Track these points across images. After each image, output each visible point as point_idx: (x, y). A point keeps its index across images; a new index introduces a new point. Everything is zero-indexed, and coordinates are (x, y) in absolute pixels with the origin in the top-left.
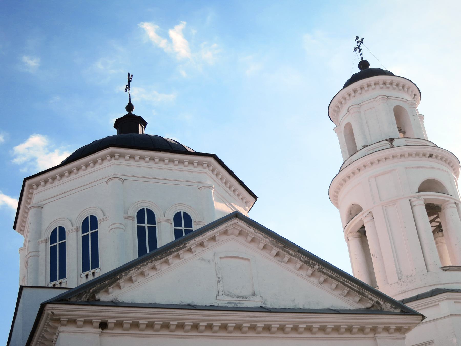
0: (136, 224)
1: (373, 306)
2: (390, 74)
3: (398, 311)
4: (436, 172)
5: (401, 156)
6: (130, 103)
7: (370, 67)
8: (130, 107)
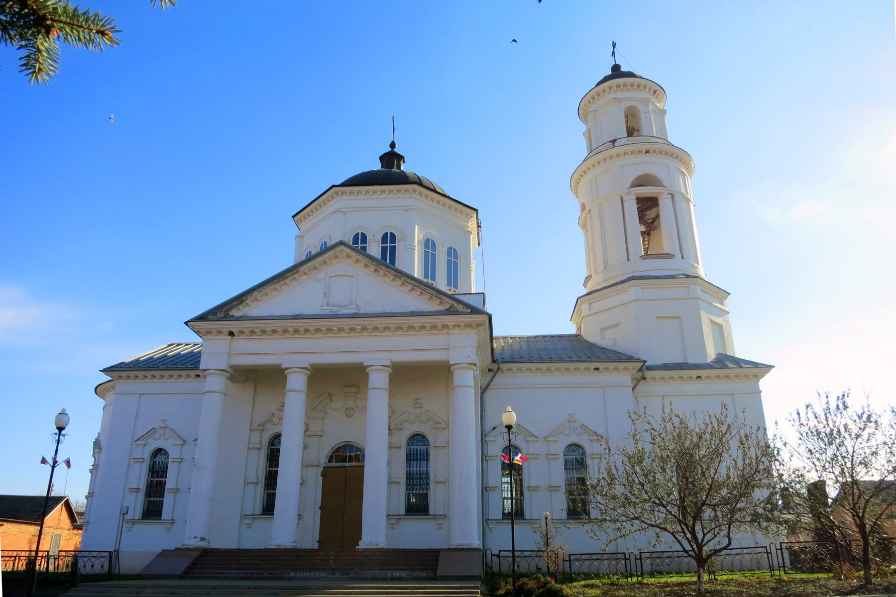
1: (451, 307)
3: (469, 311)
5: (632, 153)
8: (393, 145)
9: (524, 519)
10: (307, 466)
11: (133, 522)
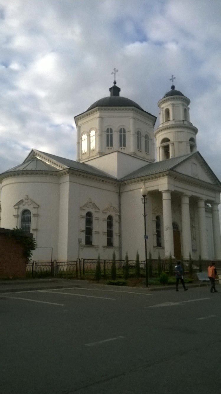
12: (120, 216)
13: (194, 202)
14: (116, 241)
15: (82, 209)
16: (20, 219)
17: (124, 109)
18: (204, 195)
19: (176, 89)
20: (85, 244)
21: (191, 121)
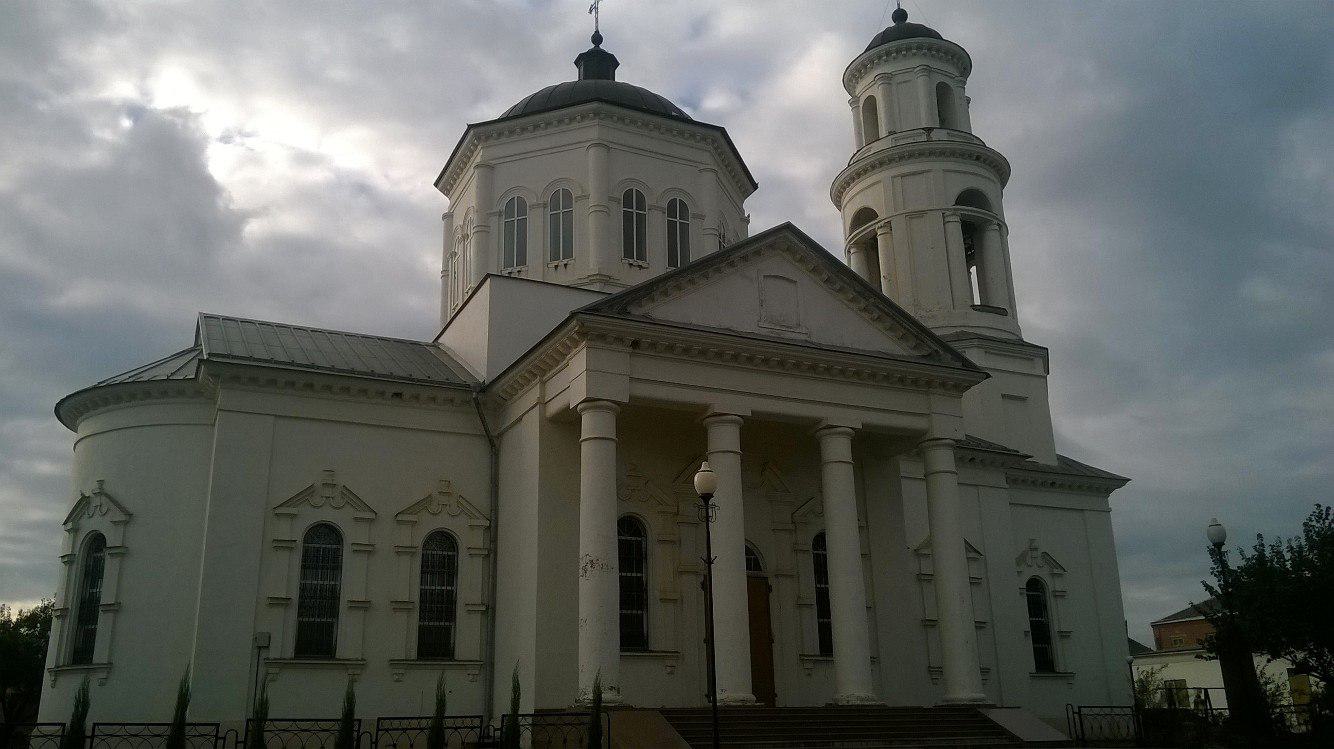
0: (666, 219)
2: (937, 36)
4: (983, 183)
6: (597, 32)
7: (908, 21)
8: (597, 38)
9: (1054, 671)
10: (792, 576)
11: (282, 664)
12: (492, 531)
13: (780, 451)
14: (467, 635)
15: (282, 511)
16: (77, 567)
17: (675, 133)
18: (843, 410)
19: (912, 19)
20: (290, 652)
21: (977, 130)
